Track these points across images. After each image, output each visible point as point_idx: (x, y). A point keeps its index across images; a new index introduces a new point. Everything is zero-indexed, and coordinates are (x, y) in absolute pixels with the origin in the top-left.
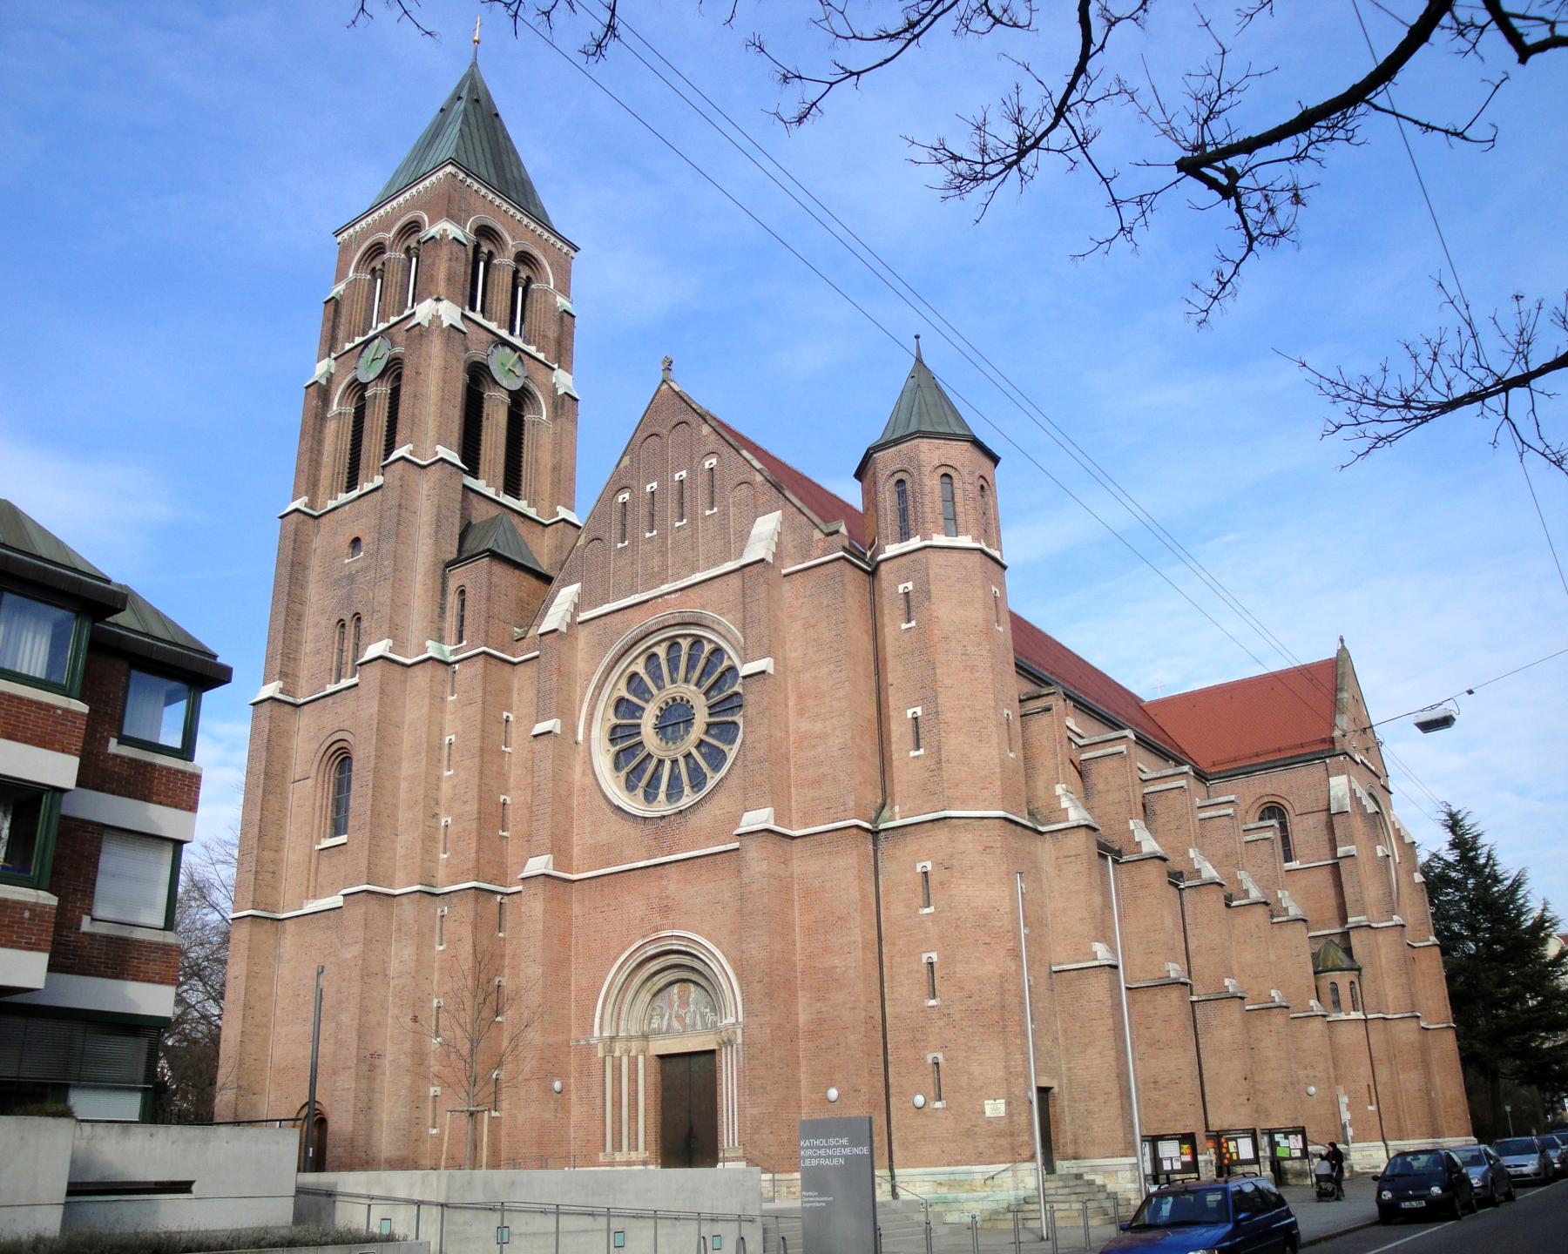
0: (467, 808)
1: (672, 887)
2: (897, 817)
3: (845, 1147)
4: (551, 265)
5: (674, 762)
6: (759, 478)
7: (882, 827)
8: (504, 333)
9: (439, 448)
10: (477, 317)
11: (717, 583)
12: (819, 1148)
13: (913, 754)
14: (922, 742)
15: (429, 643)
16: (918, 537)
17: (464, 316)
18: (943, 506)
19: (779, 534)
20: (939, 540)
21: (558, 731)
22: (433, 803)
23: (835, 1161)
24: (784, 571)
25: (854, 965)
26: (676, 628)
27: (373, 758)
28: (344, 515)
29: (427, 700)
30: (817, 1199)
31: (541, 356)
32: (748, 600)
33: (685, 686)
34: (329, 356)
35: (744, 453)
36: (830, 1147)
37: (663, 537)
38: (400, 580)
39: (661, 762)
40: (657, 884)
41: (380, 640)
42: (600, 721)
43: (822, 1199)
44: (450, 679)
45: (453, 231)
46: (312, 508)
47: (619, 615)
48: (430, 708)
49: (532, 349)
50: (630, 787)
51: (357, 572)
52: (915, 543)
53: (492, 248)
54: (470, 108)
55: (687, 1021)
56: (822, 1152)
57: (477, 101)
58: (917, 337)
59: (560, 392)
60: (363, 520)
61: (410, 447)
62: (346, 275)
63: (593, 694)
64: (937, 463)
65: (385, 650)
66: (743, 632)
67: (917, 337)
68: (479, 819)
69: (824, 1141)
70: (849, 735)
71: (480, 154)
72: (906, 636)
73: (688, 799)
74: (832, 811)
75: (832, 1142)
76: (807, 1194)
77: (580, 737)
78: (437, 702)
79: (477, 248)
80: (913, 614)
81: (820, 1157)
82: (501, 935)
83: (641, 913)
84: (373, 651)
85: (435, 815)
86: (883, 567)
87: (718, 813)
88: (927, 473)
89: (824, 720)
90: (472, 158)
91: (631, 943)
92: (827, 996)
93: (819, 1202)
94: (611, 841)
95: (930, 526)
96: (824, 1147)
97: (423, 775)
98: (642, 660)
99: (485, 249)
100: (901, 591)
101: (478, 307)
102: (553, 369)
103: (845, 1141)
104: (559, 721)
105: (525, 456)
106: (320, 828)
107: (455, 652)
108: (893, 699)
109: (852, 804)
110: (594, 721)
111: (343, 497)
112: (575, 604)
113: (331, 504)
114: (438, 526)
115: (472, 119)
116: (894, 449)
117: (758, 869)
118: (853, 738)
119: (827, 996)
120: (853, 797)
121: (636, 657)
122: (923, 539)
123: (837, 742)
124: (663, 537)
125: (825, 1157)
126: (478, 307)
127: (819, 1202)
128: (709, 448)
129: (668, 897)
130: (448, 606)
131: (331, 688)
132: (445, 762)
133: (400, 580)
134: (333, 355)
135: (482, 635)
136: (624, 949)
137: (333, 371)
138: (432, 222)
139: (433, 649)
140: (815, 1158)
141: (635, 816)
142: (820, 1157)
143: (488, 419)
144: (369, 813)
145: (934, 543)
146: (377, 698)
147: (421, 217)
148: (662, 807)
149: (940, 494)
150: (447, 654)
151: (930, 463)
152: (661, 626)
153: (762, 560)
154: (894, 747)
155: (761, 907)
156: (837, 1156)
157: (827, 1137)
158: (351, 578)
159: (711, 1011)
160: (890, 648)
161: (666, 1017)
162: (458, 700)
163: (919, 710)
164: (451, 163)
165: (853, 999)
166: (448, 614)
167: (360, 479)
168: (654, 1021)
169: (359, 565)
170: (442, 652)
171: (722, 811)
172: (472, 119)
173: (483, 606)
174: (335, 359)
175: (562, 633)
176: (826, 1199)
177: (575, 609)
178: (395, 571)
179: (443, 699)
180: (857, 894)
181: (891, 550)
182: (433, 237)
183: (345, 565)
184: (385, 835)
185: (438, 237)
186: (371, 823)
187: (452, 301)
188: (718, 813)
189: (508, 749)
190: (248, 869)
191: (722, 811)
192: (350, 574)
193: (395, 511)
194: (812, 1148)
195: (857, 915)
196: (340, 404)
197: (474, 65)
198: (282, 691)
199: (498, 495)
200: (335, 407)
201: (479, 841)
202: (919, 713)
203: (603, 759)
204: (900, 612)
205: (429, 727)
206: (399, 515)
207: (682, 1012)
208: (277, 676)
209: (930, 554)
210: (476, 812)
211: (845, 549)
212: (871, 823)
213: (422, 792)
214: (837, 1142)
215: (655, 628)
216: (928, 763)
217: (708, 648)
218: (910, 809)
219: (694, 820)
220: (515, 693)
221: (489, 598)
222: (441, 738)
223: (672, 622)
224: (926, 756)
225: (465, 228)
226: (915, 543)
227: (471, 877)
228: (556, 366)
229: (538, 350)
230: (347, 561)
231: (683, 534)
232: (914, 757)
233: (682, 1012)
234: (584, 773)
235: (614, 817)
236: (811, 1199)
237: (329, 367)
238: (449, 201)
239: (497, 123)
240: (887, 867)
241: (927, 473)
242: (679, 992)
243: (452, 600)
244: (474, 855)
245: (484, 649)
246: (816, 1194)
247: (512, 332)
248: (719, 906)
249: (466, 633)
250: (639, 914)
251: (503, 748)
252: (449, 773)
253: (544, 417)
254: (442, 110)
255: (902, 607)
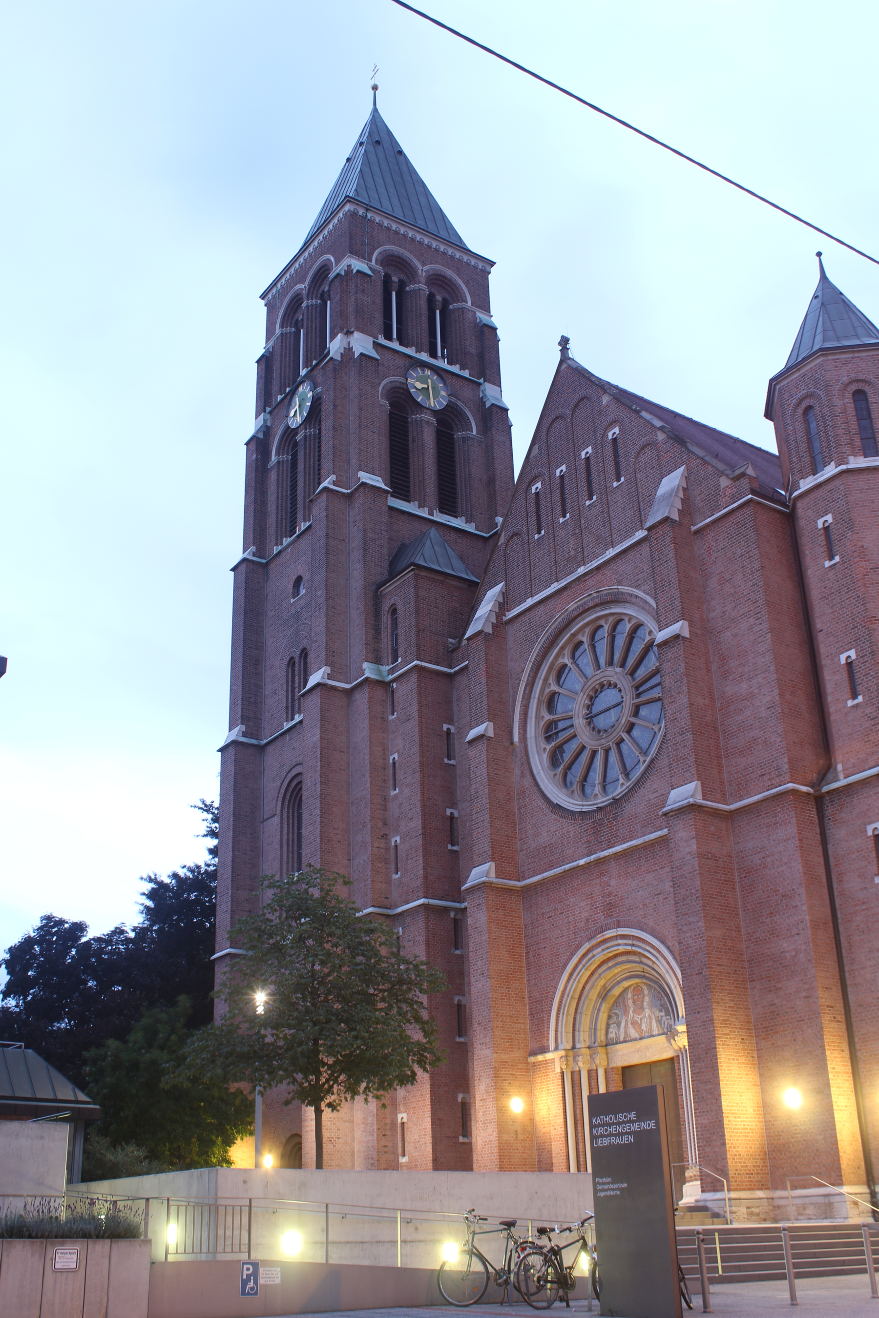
0: (412, 824)
1: (613, 883)
2: (841, 776)
3: (631, 1121)
4: (467, 283)
5: (607, 751)
6: (661, 436)
7: (825, 789)
8: (424, 356)
9: (361, 474)
10: (395, 345)
11: (630, 555)
12: (610, 1125)
13: (850, 703)
14: (859, 688)
15: (365, 665)
16: (833, 463)
17: (376, 345)
18: (859, 424)
19: (684, 489)
20: (858, 462)
21: (491, 733)
22: (380, 824)
23: (625, 1138)
24: (693, 528)
25: (803, 947)
26: (597, 609)
27: (318, 785)
28: (288, 557)
29: (367, 722)
30: (612, 1186)
31: (466, 373)
32: (657, 564)
33: (610, 669)
34: (265, 411)
35: (644, 414)
36: (619, 1124)
37: (577, 517)
38: (334, 608)
39: (594, 753)
40: (598, 881)
41: (319, 669)
42: (533, 719)
43: (616, 1186)
44: (390, 699)
45: (358, 265)
46: (260, 557)
47: (541, 608)
48: (371, 729)
49: (455, 369)
50: (565, 782)
51: (302, 609)
52: (831, 470)
53: (403, 277)
54: (371, 149)
55: (644, 1027)
56: (612, 1129)
57: (378, 142)
58: (819, 254)
59: (488, 405)
60: (303, 558)
61: (333, 477)
62: (273, 334)
63: (524, 693)
64: (845, 379)
65: (323, 678)
66: (655, 598)
67: (819, 254)
68: (424, 834)
69: (613, 1118)
70: (776, 691)
71: (382, 190)
72: (831, 574)
73: (618, 791)
74: (766, 778)
75: (621, 1117)
76: (601, 1181)
77: (516, 739)
78: (379, 723)
79: (387, 280)
80: (836, 548)
81: (611, 1135)
82: (458, 952)
83: (586, 914)
84: (313, 680)
85: (385, 836)
86: (799, 505)
87: (652, 796)
88: (836, 393)
89: (749, 679)
90: (374, 195)
91: (578, 947)
92: (780, 985)
93: (613, 1190)
94: (552, 841)
95: (846, 449)
96: (614, 1124)
97: (368, 797)
98: (567, 652)
99: (439, 298)
100: (820, 526)
101: (395, 336)
102: (480, 384)
103: (632, 1116)
104: (492, 724)
105: (458, 473)
106: (288, 863)
107: (392, 671)
108: (824, 648)
109: (786, 766)
110: (529, 721)
111: (286, 541)
112: (500, 604)
113: (276, 550)
114: (365, 550)
115: (373, 158)
116: (798, 374)
117: (687, 850)
118: (781, 695)
119: (780, 985)
120: (786, 760)
121: (563, 648)
122: (837, 466)
123: (764, 701)
124: (577, 517)
125: (615, 1135)
126: (395, 336)
127: (613, 1190)
128: (611, 417)
129: (610, 894)
130: (383, 626)
131: (287, 726)
132: (391, 782)
133: (334, 608)
134: (268, 409)
135: (414, 649)
136: (572, 955)
137: (269, 424)
138: (338, 261)
139: (369, 671)
140: (606, 1136)
141: (573, 813)
142: (611, 1135)
143: (414, 441)
144: (318, 840)
145: (850, 466)
146: (319, 725)
147: (330, 260)
148: (602, 800)
149: (854, 413)
150: (386, 673)
151: (837, 381)
152: (581, 610)
153: (666, 519)
154: (830, 699)
155: (693, 891)
156: (627, 1133)
157: (615, 1113)
158: (297, 616)
159: (666, 1015)
160: (815, 592)
161: (623, 1025)
162: (398, 718)
163: (852, 654)
164: (348, 201)
165: (807, 986)
166: (383, 635)
167: (298, 520)
168: (610, 1030)
169: (302, 602)
170: (380, 672)
171: (656, 794)
172: (373, 158)
173: (413, 621)
174: (270, 413)
175: (487, 634)
176: (620, 1185)
177: (500, 608)
178: (327, 600)
179: (384, 719)
180: (800, 866)
181: (806, 484)
182: (338, 275)
183: (292, 605)
184: (337, 861)
185: (343, 273)
186: (321, 850)
187: (362, 332)
188: (652, 796)
189: (452, 762)
190: (225, 909)
191: (656, 794)
192: (297, 612)
193: (323, 541)
194: (603, 1125)
195: (802, 890)
196: (278, 454)
197: (375, 110)
198: (244, 734)
199: (431, 514)
200: (274, 458)
201: (425, 856)
202: (854, 657)
203: (539, 762)
204: (822, 549)
205: (371, 748)
206: (327, 545)
207: (638, 1018)
208: (239, 721)
209: (850, 478)
210: (420, 827)
211: (753, 492)
212: (812, 787)
213: (369, 813)
214: (626, 1117)
215: (575, 613)
216: (868, 710)
217: (627, 627)
218: (854, 766)
219: (630, 809)
220: (455, 704)
221: (417, 612)
222: (385, 757)
223: (591, 604)
224: (865, 703)
225: (370, 261)
226: (831, 470)
227: (421, 894)
228: (482, 381)
229: (462, 368)
230: (292, 601)
231: (595, 511)
232: (853, 707)
233: (638, 1018)
234: (523, 776)
235: (554, 816)
236: (605, 1187)
237: (265, 421)
238: (351, 238)
239: (401, 158)
240: (839, 834)
241: (836, 393)
242: (633, 996)
243: (386, 619)
244: (421, 872)
245: (416, 662)
246: (610, 1180)
247: (433, 355)
248: (661, 897)
249: (401, 651)
250: (585, 915)
251: (446, 761)
252: (395, 792)
253: (474, 432)
254: (348, 160)
255: (824, 543)
